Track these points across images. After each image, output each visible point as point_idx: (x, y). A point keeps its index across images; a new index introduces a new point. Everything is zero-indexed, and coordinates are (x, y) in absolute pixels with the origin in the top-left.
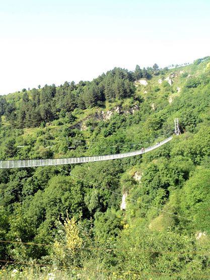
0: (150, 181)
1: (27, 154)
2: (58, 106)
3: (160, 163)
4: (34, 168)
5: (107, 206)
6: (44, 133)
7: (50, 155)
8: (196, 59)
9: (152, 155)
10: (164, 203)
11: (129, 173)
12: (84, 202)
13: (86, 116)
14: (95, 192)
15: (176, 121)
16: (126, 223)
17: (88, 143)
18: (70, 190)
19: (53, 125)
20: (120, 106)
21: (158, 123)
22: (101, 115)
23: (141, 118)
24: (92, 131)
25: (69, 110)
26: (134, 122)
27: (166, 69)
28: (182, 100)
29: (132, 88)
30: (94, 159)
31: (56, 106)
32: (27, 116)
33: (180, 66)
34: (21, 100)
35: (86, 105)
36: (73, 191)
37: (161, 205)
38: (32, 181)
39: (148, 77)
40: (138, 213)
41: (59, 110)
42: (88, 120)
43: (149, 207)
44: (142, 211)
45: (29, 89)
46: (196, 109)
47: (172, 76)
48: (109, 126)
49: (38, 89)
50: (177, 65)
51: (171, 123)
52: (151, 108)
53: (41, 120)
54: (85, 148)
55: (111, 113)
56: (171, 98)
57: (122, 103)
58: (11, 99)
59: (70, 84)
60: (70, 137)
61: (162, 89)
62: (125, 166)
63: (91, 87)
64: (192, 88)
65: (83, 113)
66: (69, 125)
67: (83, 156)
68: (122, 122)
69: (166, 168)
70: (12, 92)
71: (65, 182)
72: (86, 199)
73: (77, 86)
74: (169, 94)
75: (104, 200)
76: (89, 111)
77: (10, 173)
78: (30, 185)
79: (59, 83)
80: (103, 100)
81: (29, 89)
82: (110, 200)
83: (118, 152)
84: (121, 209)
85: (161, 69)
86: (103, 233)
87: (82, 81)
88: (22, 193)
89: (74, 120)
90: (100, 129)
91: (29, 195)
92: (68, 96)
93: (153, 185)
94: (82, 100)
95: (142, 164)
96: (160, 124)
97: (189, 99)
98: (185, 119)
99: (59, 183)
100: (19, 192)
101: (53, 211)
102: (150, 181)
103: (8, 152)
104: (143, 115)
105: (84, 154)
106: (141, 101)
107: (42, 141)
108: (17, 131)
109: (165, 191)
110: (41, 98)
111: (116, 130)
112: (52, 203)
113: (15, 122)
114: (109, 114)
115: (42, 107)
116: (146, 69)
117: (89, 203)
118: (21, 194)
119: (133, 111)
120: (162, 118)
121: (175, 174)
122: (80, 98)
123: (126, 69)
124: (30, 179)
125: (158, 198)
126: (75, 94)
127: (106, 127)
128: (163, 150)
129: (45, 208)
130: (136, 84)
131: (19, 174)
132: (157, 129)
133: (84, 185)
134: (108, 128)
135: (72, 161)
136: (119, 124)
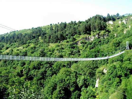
0: (111, 73)
1: (50, 56)
2: (67, 33)
5: (88, 85)
7: (61, 57)
9: (113, 60)
10: (118, 86)
11: (101, 68)
12: (76, 82)
14: (83, 77)
15: (127, 43)
16: (98, 94)
19: (64, 42)
20: (98, 34)
21: (117, 43)
22: (89, 38)
23: (109, 41)
24: (84, 46)
25: (72, 35)
27: (123, 16)
29: (105, 25)
31: (66, 33)
32: (51, 37)
33: (131, 15)
34: (49, 29)
35: (81, 33)
36: (72, 76)
37: (116, 86)
38: (51, 70)
39: (114, 20)
40: (104, 90)
41: (67, 35)
44: (106, 89)
47: (127, 20)
48: (92, 44)
49: (58, 24)
51: (125, 44)
52: (114, 36)
53: (58, 39)
57: (100, 33)
58: (44, 29)
59: (74, 22)
61: (121, 26)
62: (99, 65)
63: (84, 24)
66: (72, 43)
72: (78, 80)
74: (124, 29)
75: (87, 82)
76: (82, 36)
77: (41, 65)
78: (50, 71)
80: (90, 31)
82: (90, 81)
84: (96, 87)
87: (80, 21)
88: (46, 75)
89: (75, 40)
90: (87, 45)
91: (49, 76)
92: (72, 28)
94: (79, 30)
95: (108, 64)
99: (65, 71)
100: (45, 75)
101: (61, 86)
102: (111, 73)
103: (41, 54)
108: (46, 45)
109: (119, 79)
112: (60, 81)
114: (92, 38)
116: (113, 16)
117: (79, 83)
118: (45, 75)
119: (105, 37)
120: (120, 41)
121: (125, 70)
123: (102, 15)
124: (50, 68)
125: (115, 83)
126: (76, 27)
127: (91, 44)
128: (120, 57)
129: (57, 84)
130: (107, 23)
131: (45, 65)
134: (91, 45)
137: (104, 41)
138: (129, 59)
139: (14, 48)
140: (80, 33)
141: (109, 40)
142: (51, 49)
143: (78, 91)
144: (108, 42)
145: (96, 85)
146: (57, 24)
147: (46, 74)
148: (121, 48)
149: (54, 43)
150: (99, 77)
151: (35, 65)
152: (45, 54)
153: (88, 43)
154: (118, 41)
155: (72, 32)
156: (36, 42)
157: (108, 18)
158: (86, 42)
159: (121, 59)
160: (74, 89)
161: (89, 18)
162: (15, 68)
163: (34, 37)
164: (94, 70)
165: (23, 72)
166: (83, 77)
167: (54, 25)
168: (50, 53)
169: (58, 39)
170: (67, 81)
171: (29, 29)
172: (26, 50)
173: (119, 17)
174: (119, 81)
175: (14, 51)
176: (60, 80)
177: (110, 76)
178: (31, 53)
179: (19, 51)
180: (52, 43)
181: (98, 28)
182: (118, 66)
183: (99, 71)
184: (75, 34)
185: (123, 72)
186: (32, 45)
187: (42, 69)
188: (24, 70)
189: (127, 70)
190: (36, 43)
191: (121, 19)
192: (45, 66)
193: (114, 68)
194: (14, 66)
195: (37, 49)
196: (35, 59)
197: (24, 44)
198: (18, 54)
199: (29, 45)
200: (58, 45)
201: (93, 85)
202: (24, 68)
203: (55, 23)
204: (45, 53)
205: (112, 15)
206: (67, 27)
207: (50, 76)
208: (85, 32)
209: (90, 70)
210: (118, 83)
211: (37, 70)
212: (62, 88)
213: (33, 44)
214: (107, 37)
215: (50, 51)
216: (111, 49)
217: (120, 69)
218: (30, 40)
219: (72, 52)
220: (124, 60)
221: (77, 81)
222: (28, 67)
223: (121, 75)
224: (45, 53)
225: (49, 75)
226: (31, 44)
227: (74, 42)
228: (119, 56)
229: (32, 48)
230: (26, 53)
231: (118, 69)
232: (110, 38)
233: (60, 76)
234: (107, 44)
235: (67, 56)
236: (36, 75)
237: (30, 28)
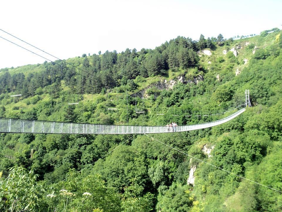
0: (224, 155)
1: (86, 120)
2: (120, 73)
3: (235, 137)
4: (94, 136)
5: (172, 180)
6: (105, 100)
7: (111, 122)
8: (263, 30)
9: (223, 128)
10: (239, 181)
11: (197, 145)
12: (147, 175)
13: (148, 85)
14: (160, 164)
15: (247, 92)
16: (195, 199)
17: (150, 112)
18: (133, 161)
19: (114, 92)
20: (184, 76)
21: (227, 94)
22: (164, 84)
23: (206, 88)
24: (154, 100)
25: (132, 78)
26: (198, 92)
27: (232, 40)
28: (251, 71)
29: (196, 58)
30: (156, 130)
31: (118, 72)
32: (88, 82)
33: (245, 37)
34: (81, 65)
35: (149, 73)
36: (137, 162)
37: (236, 181)
38: (92, 149)
39: (213, 47)
40: (210, 189)
41: (120, 77)
42: (149, 89)
43: (222, 184)
44: (215, 187)
45: (89, 55)
46: (267, 82)
47: (238, 47)
48: (172, 95)
49: (99, 54)
50: (243, 37)
51: (241, 94)
52: (215, 79)
53: (102, 86)
54: (148, 118)
55: (174, 83)
56: (238, 70)
57: (186, 72)
59: (131, 52)
60: (132, 105)
61: (227, 60)
62: (193, 138)
64: (261, 60)
65: (145, 81)
66: (131, 93)
67: (146, 126)
68: (186, 92)
69: (242, 142)
70: (71, 58)
71: (128, 152)
72: (150, 171)
73: (138, 54)
74: (234, 65)
75: (169, 173)
76: (151, 79)
77: (69, 140)
78: (89, 152)
79: (120, 50)
80: (167, 68)
81: (89, 55)
82: (177, 172)
83: (185, 123)
84: (188, 184)
85: (226, 39)
86: (170, 209)
87: (144, 49)
88: (81, 160)
89: (136, 88)
90: (162, 98)
91: (88, 163)
92: (130, 63)
93: (227, 160)
94: (144, 68)
95: (211, 137)
96: (229, 95)
97: (260, 71)
98: (256, 91)
99: (122, 152)
100: (78, 160)
101: (115, 182)
102: (224, 155)
103: (67, 117)
104: (207, 86)
105: (147, 123)
106: (205, 71)
107: (102, 107)
108: (77, 97)
109: (241, 166)
110: (102, 64)
111: (179, 100)
112: (114, 173)
113: (75, 87)
114: (172, 83)
115: (103, 74)
116: (210, 39)
117: (154, 176)
118: (79, 162)
119: (197, 81)
120: (231, 89)
121: (252, 148)
122: (142, 66)
123: (190, 38)
124: (89, 147)
125: (233, 174)
126: (137, 61)
127: (169, 96)
128: (237, 123)
129: (107, 179)
130: (200, 54)
131: (78, 140)
132: (226, 100)
133: (148, 156)
134: (171, 98)
135: (133, 130)
136: (183, 94)
137: (195, 89)
138: (257, 125)
139: (8, 103)
140: (147, 73)
141: (205, 87)
142: (89, 106)
143: (152, 193)
144: (205, 91)
145: (189, 178)
146: (97, 54)
147: (80, 158)
148: (235, 104)
149: (94, 93)
150: (196, 163)
151: (58, 139)
152: (75, 117)
153: (163, 94)
154: (227, 89)
155: (129, 71)
156: (55, 90)
157: (201, 43)
158: (160, 91)
159: (240, 127)
160: (143, 189)
161: (164, 44)
162: (12, 147)
163: (50, 82)
164: (184, 148)
165: (31, 154)
166: (161, 163)
167: (91, 56)
168: (86, 113)
169: (102, 85)
170: (128, 172)
171: (39, 65)
172: (34, 109)
173: (222, 43)
174: (241, 169)
175: (7, 110)
176: (114, 172)
177: (220, 161)
178: (46, 114)
179: (19, 111)
180: (90, 93)
181: (183, 63)
182: (236, 140)
183: (195, 150)
184: (137, 76)
185: (247, 152)
186: (47, 98)
187: (71, 147)
188: (32, 150)
189: (256, 147)
190: (56, 93)
191: (228, 46)
192: (79, 142)
193: (230, 144)
194: (10, 143)
195: (57, 106)
196: (60, 129)
197: (28, 96)
198: (17, 116)
199: (39, 99)
200: (102, 99)
201: (183, 179)
202: (33, 146)
203: (94, 53)
204: (76, 115)
205: (209, 38)
206: (118, 61)
207: (89, 163)
208: (156, 72)
209: (176, 148)
210: (238, 174)
211: (61, 151)
212: (118, 188)
213: (48, 94)
214: (202, 81)
215: (86, 110)
216: (216, 106)
217: (241, 146)
218: (42, 87)
219: (132, 113)
220: (245, 127)
221: (148, 171)
222: (42, 144)
223: (244, 159)
224: (76, 115)
225: (87, 161)
226: (44, 96)
227: (134, 91)
228: (235, 120)
229: (47, 104)
230: (35, 114)
231: (238, 145)
232: (207, 83)
233: (113, 162)
234: (201, 95)
235: (121, 120)
236: (59, 161)
237: (40, 63)
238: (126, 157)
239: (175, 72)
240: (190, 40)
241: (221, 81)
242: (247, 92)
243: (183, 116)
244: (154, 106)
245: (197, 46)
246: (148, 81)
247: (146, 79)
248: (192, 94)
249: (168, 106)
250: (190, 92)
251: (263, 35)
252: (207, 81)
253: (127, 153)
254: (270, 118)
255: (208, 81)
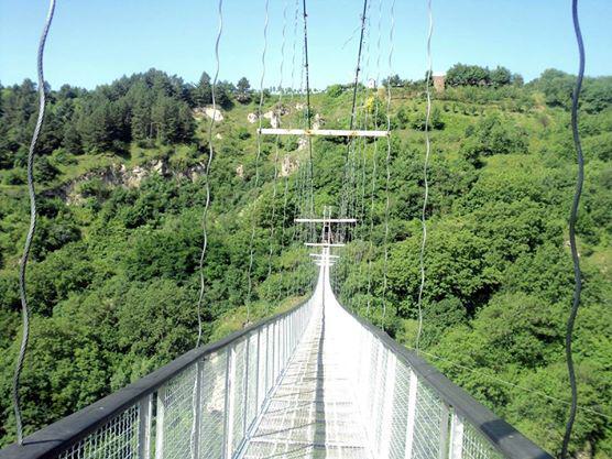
13: (84, 172)
20: (166, 160)
22: (119, 175)
24: (97, 209)
27: (267, 95)
35: (85, 144)
39: (226, 104)
42: (86, 182)
48: (138, 202)
52: (234, 174)
60: (45, 218)
73: (54, 96)
74: (270, 148)
76: (89, 161)
80: (126, 136)
89: (53, 177)
90: (115, 206)
104: (217, 188)
114: (136, 173)
119: (194, 174)
123: (178, 77)
127: (132, 204)
136: (164, 201)
227: (49, 183)
232: (215, 180)
238: (54, 348)
239: (145, 148)
240: (180, 81)
241: (248, 179)
242: (328, 210)
243: (187, 253)
244: (94, 223)
245: (193, 98)
246: (82, 164)
247: (77, 158)
248: (184, 204)
249: (129, 226)
250: (180, 199)
251: (333, 93)
252: (215, 177)
253: (54, 336)
254: (399, 271)
255: (219, 175)
